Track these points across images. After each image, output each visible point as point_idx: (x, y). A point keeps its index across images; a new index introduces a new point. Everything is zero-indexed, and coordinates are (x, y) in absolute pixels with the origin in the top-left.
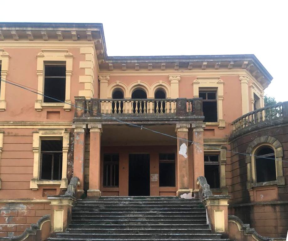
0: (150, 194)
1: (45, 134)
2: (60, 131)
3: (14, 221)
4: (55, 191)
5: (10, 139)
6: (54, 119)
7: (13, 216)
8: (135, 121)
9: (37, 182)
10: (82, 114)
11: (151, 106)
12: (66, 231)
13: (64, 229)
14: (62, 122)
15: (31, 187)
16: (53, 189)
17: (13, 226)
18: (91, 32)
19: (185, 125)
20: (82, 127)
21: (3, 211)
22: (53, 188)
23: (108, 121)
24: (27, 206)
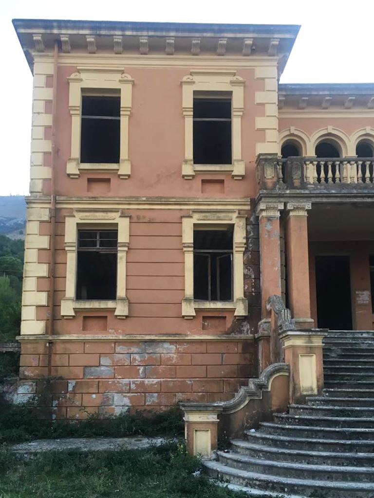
1: (204, 220)
2: (230, 214)
3: (156, 374)
4: (222, 321)
5: (141, 229)
6: (213, 193)
7: (153, 364)
9: (194, 304)
10: (275, 185)
11: (311, 173)
15: (183, 314)
16: (219, 317)
18: (41, 35)
20: (277, 208)
21: (134, 355)
22: (220, 315)
23: (322, 197)
24: (176, 346)
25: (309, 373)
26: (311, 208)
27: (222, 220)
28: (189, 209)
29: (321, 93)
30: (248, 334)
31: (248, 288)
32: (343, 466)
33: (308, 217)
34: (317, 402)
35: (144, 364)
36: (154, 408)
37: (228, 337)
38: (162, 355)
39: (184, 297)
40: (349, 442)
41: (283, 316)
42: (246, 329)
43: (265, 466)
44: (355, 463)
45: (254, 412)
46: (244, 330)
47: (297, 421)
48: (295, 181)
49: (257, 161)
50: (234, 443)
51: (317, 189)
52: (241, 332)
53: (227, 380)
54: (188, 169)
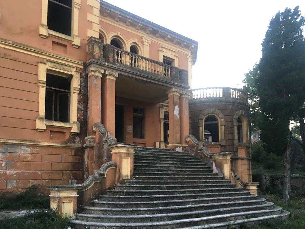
0: (156, 146)
1: (54, 68)
2: (71, 68)
3: (15, 167)
4: (62, 135)
6: (59, 52)
8: (144, 77)
9: (46, 122)
12: (133, 178)
13: (131, 176)
14: (72, 58)
15: (37, 127)
16: (61, 132)
17: (14, 173)
19: (178, 90)
20: (100, 72)
22: (62, 131)
25: (127, 168)
26: (118, 76)
27: (66, 71)
28: (44, 59)
29: (116, 12)
30: (78, 144)
31: (79, 117)
32: (155, 214)
33: (116, 81)
34: (132, 183)
35: (6, 160)
36: (13, 191)
37: (66, 145)
38: (20, 154)
39: (38, 116)
40: (155, 202)
41: (107, 135)
42: (77, 141)
43: (116, 218)
44: (160, 212)
45: (97, 190)
46: (76, 142)
47: (124, 193)
48: (110, 59)
49: (88, 40)
50: (85, 208)
51: (120, 67)
52: (74, 142)
53: (65, 172)
54: (44, 31)
